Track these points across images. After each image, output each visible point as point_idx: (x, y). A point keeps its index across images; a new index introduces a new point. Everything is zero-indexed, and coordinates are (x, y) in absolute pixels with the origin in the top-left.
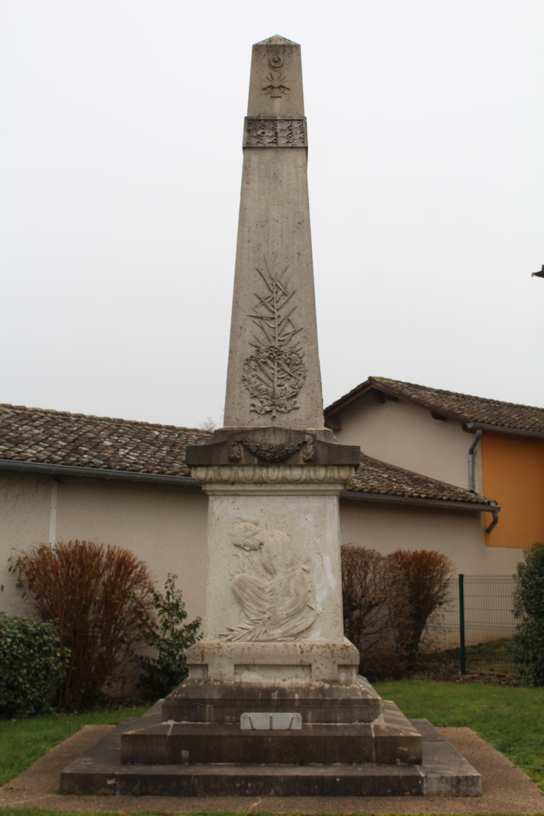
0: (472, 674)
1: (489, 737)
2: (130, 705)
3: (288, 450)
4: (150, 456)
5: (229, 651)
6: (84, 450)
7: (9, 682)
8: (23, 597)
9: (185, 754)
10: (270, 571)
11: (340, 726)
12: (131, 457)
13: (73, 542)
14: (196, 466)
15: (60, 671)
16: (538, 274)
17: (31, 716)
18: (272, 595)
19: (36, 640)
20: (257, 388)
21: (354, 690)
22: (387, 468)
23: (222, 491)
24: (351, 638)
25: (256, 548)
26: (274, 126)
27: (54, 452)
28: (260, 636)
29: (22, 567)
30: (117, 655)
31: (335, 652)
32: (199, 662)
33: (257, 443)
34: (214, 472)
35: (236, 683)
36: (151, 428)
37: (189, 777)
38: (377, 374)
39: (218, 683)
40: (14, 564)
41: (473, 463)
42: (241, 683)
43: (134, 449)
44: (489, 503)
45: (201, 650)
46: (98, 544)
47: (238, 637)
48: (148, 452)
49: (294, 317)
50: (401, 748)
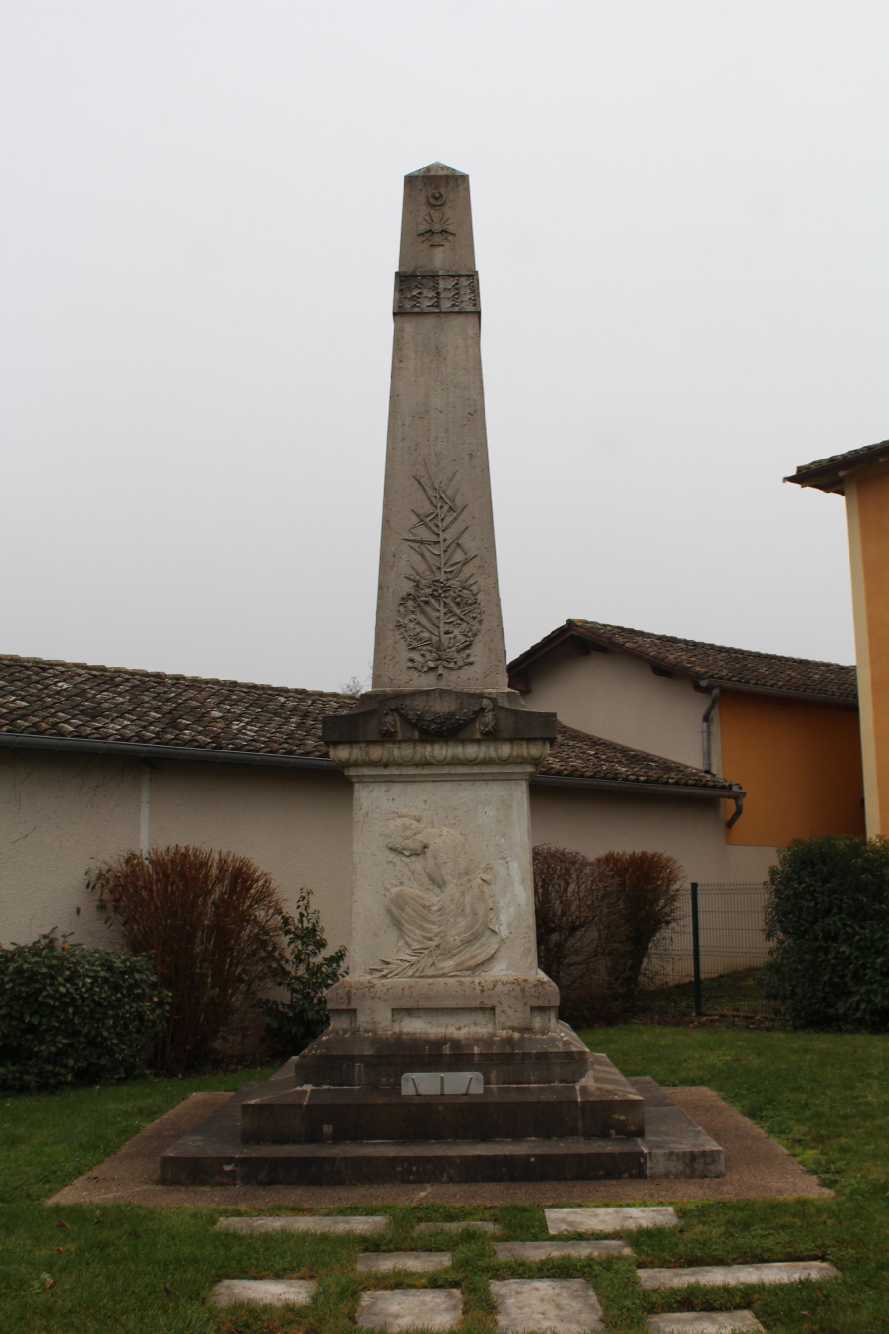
1: (734, 1098)
3: (459, 720)
8: (106, 923)
10: (438, 883)
12: (249, 733)
14: (336, 743)
15: (158, 1021)
16: (791, 479)
17: (120, 1081)
18: (441, 915)
19: (125, 980)
20: (416, 637)
21: (553, 1040)
22: (594, 742)
27: (144, 727)
28: (425, 971)
29: (104, 882)
30: (234, 999)
31: (527, 989)
32: (344, 1007)
33: (418, 710)
35: (395, 1033)
36: (275, 693)
37: (333, 1159)
38: (578, 615)
39: (371, 1034)
40: (94, 879)
41: (709, 733)
42: (401, 1033)
43: (252, 721)
44: (730, 786)
45: (346, 990)
46: (205, 849)
50: (616, 1116)
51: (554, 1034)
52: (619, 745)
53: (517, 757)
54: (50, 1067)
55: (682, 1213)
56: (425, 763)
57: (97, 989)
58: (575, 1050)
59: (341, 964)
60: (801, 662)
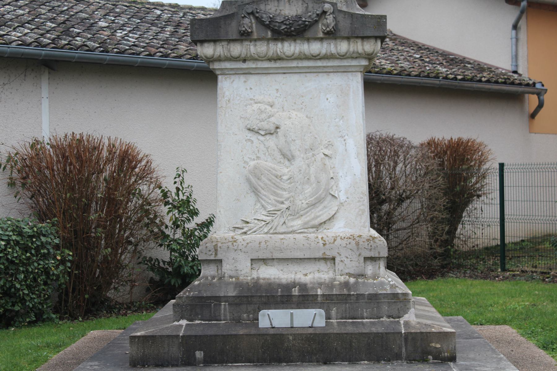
0: (513, 271)
1: (531, 335)
2: (139, 309)
3: (305, 21)
4: (152, 37)
5: (245, 245)
6: (76, 32)
7: (5, 289)
8: (16, 197)
9: (199, 355)
10: (288, 157)
11: (367, 322)
12: (130, 39)
13: (69, 134)
14: (202, 42)
15: (61, 276)
17: (31, 324)
18: (291, 183)
19: (33, 243)
21: (382, 284)
22: (419, 47)
23: (232, 69)
24: (379, 231)
25: (272, 132)
27: (42, 35)
28: (278, 228)
29: (13, 164)
30: (123, 257)
31: (361, 243)
32: (212, 258)
33: (271, 14)
34: (223, 48)
35: (253, 279)
36: (152, 7)
39: (234, 279)
41: (517, 40)
42: (258, 278)
43: (133, 30)
44: (534, 84)
45: (214, 244)
46: (96, 135)
47: (255, 229)
48: (150, 33)
50: (433, 345)
51: (382, 279)
52: (441, 50)
53: (353, 53)
56: (278, 58)
57: (10, 250)
58: (400, 292)
59: (211, 228)
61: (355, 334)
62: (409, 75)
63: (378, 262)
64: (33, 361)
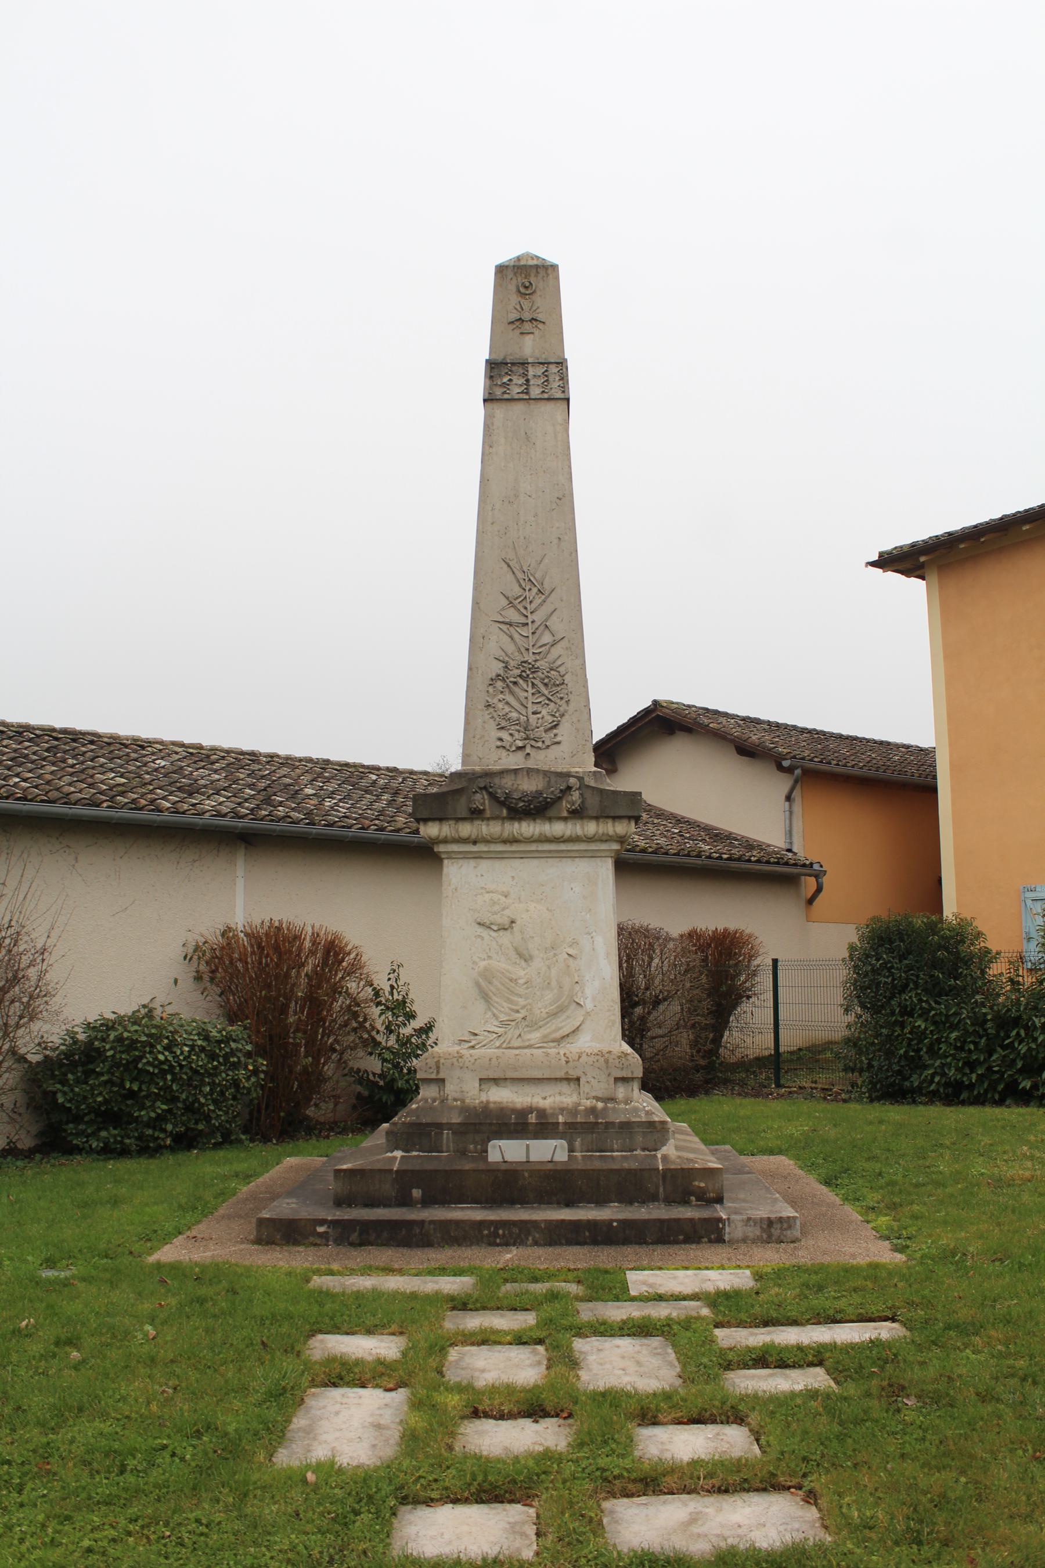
0: (789, 1087)
1: (810, 1167)
2: (344, 1131)
9: (417, 1193)
10: (525, 957)
14: (426, 820)
16: (873, 564)
17: (217, 1146)
18: (527, 988)
19: (221, 1049)
20: (505, 717)
21: (636, 1110)
22: (679, 820)
26: (525, 373)
27: (239, 804)
30: (326, 1068)
31: (611, 1061)
32: (433, 1076)
38: (662, 696)
40: (191, 951)
41: (791, 813)
42: (488, 1102)
44: (811, 864)
46: (298, 923)
49: (554, 623)
50: (696, 1183)
54: (150, 1132)
55: (758, 1276)
56: (514, 841)
58: (657, 1119)
59: (430, 1034)
60: (881, 743)
61: (604, 1170)
62: (666, 853)
63: (631, 1083)
64: (220, 1194)
